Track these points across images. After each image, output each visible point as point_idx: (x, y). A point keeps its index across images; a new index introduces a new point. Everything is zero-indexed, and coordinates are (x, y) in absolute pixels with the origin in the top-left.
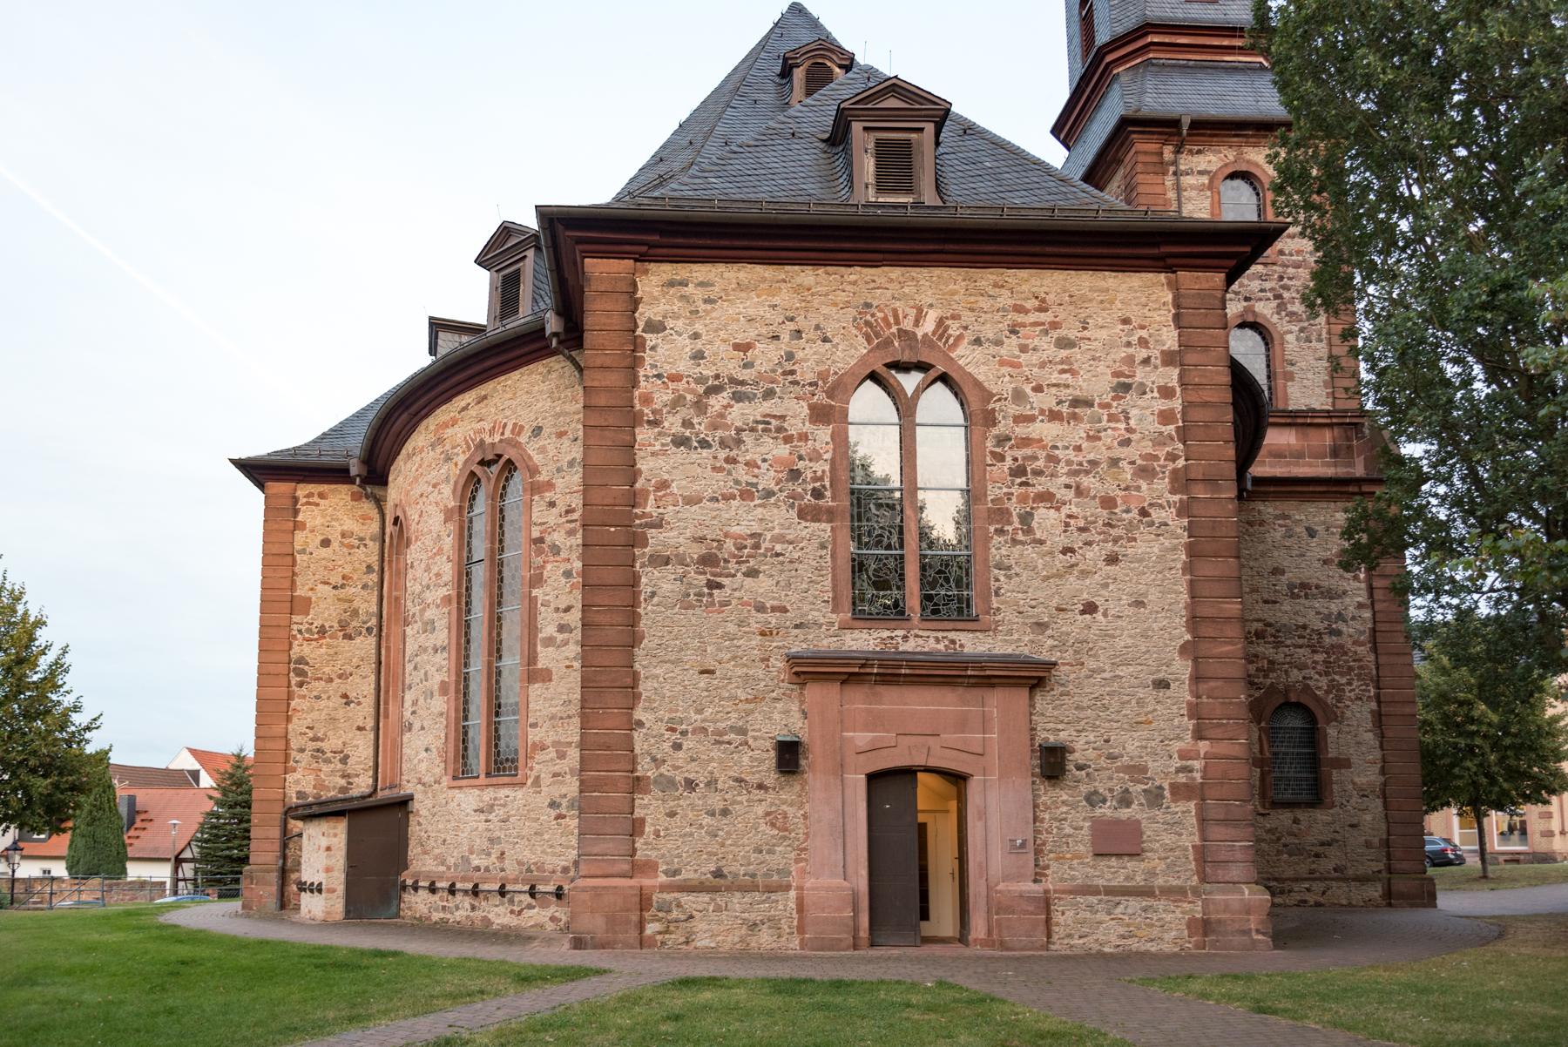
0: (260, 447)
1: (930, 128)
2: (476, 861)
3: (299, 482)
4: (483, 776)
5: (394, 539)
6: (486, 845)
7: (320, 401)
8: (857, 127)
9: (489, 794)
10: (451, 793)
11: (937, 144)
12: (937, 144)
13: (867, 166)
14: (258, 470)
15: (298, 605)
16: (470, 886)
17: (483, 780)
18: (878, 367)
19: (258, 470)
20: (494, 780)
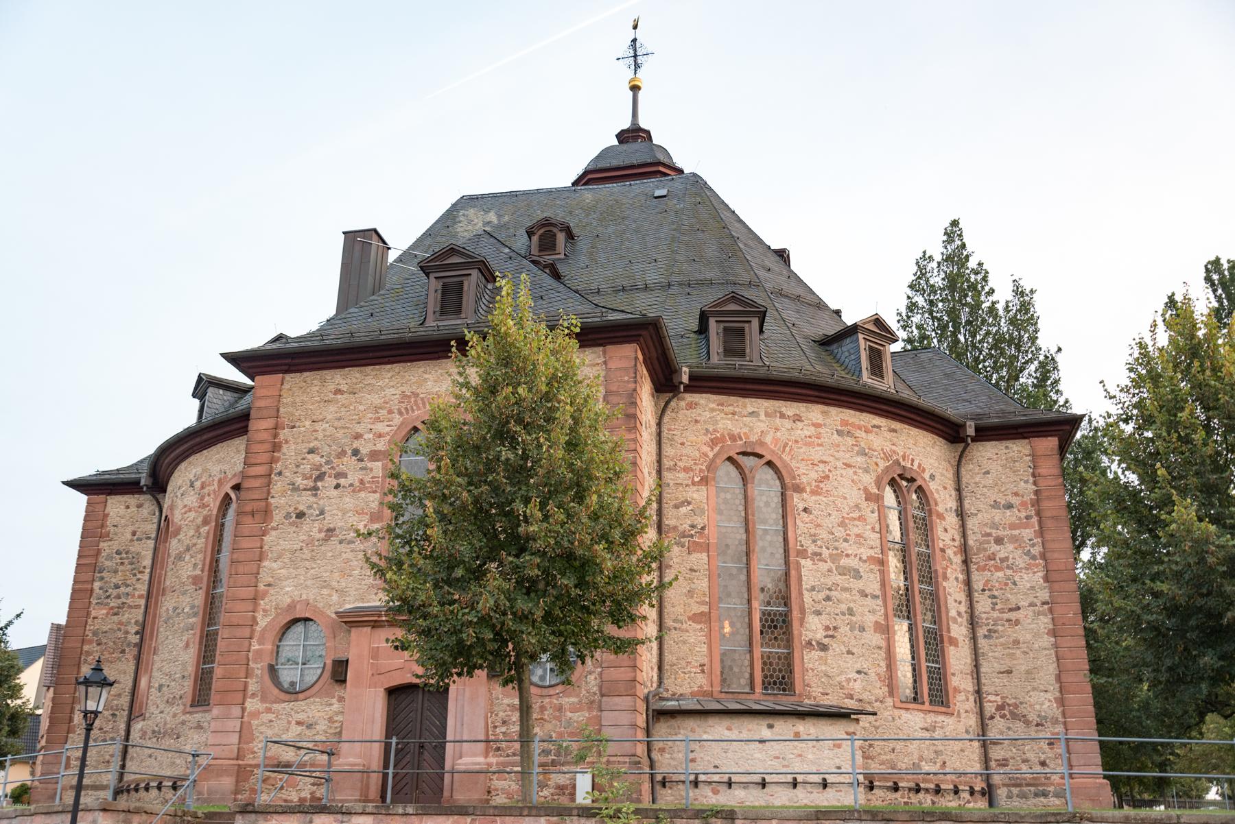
0: (85, 470)
1: (755, 322)
2: (926, 768)
3: (109, 494)
4: (927, 703)
5: (164, 529)
6: (932, 755)
7: (130, 449)
8: (712, 322)
9: (931, 718)
10: (897, 712)
11: (761, 331)
12: (761, 331)
13: (716, 344)
14: (77, 485)
15: (95, 568)
16: (932, 786)
17: (927, 706)
18: (732, 454)
19: (77, 485)
20: (936, 708)
